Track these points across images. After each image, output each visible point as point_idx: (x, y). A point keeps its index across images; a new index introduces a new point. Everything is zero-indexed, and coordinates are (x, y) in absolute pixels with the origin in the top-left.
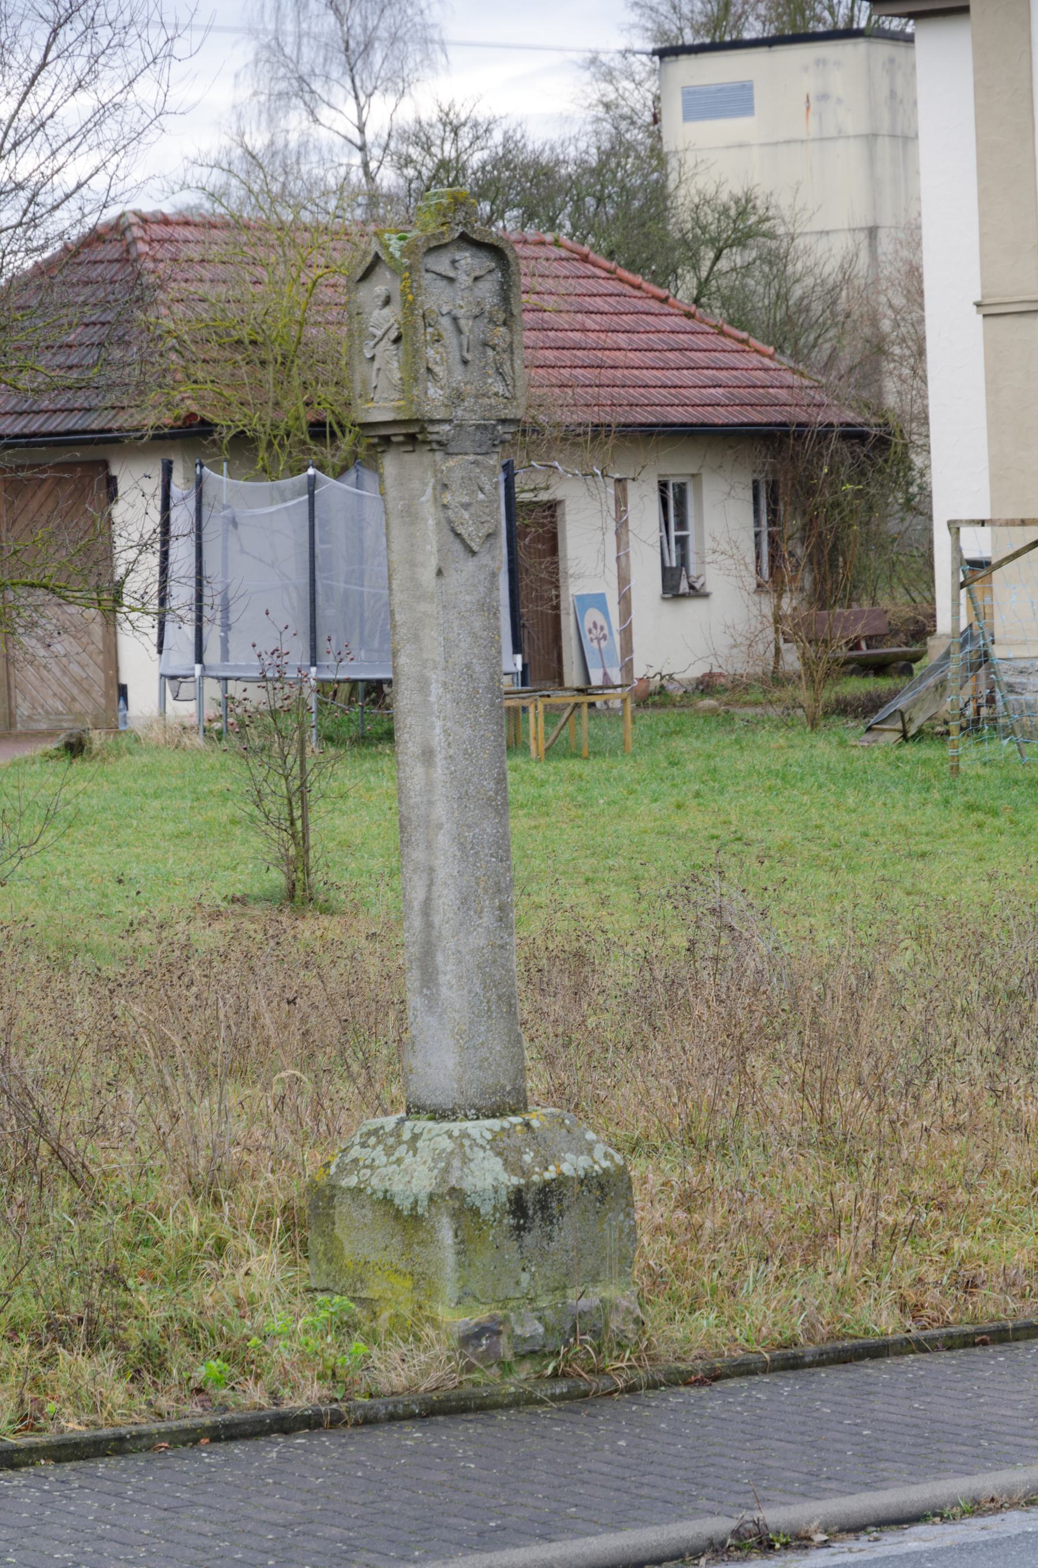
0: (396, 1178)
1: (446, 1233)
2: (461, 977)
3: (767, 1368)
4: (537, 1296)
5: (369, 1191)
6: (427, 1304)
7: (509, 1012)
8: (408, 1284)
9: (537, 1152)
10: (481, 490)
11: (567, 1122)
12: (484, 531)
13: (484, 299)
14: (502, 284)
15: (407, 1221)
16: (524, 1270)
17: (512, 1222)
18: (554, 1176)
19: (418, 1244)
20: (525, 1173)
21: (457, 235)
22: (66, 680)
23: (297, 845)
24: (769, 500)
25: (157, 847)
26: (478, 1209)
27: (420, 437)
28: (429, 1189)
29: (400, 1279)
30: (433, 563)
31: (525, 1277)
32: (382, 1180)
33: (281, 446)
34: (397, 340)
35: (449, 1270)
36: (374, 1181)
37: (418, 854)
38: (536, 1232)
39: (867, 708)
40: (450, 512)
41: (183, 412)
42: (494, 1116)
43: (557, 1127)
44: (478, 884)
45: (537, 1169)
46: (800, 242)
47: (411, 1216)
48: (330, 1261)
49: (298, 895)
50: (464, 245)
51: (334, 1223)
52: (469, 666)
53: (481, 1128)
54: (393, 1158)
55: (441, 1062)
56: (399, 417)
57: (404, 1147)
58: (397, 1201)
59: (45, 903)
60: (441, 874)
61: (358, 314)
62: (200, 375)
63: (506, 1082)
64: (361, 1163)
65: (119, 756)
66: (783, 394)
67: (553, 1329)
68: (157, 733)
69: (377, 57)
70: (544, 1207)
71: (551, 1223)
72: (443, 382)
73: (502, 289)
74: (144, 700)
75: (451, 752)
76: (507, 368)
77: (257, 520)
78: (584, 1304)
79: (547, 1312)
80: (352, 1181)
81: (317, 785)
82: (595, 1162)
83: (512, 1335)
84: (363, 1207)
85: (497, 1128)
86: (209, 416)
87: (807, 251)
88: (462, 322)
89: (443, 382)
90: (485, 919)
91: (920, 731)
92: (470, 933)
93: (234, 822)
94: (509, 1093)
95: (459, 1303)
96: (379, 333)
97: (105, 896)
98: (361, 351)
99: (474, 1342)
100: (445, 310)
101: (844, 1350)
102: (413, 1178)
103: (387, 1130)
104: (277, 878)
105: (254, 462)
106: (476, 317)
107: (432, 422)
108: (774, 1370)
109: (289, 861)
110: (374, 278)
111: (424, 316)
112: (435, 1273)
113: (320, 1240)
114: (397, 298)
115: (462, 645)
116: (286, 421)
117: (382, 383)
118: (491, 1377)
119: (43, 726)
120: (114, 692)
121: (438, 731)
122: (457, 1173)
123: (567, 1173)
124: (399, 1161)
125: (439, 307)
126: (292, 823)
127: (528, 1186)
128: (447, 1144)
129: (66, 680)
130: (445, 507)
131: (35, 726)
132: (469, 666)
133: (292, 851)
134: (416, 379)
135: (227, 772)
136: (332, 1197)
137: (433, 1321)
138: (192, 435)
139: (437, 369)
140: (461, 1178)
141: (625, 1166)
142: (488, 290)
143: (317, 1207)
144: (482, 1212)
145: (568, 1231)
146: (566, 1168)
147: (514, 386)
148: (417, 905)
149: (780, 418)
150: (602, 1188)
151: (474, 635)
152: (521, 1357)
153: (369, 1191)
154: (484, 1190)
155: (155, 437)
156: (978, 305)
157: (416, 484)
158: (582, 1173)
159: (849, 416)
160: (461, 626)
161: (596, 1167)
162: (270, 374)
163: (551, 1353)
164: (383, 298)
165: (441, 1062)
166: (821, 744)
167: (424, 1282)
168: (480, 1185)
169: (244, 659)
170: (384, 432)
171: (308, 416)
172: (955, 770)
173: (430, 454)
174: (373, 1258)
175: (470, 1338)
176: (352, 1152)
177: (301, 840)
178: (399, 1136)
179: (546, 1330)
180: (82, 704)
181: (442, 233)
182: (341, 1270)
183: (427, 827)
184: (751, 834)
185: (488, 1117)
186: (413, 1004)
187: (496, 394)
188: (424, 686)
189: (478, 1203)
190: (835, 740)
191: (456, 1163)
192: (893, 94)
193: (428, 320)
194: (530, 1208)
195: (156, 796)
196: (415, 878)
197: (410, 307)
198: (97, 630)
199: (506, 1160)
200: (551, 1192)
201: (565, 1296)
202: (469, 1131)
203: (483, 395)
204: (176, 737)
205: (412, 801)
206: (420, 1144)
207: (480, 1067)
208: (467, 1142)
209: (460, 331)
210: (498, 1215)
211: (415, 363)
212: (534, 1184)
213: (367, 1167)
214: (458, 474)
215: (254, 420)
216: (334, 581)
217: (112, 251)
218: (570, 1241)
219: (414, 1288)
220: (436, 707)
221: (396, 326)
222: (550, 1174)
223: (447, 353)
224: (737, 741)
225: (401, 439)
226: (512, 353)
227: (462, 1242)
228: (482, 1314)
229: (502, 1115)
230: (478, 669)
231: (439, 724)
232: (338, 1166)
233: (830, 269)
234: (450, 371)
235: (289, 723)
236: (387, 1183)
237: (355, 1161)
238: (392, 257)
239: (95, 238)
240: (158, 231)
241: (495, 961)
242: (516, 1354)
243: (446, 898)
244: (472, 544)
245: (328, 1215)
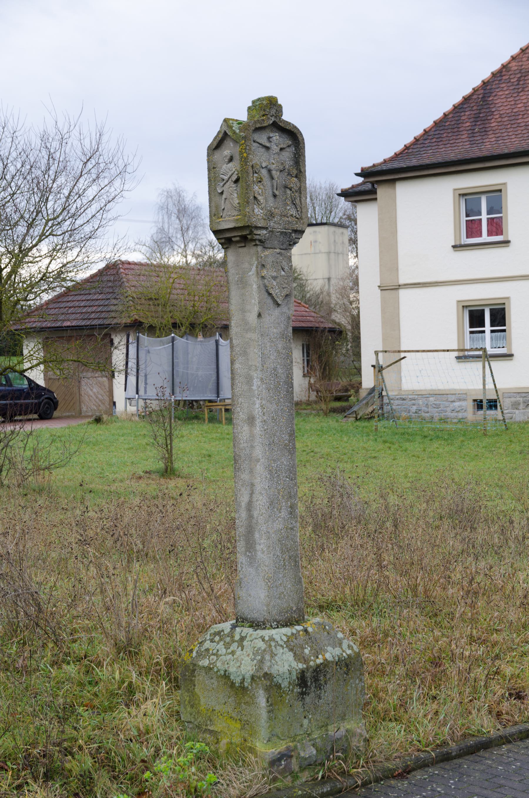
0: (232, 663)
1: (262, 700)
2: (269, 547)
3: (434, 762)
4: (312, 731)
5: (215, 670)
6: (249, 739)
7: (295, 566)
8: (238, 726)
9: (311, 647)
10: (283, 269)
11: (327, 627)
12: (284, 293)
13: (285, 161)
14: (295, 154)
15: (239, 690)
16: (305, 717)
17: (299, 690)
18: (322, 661)
19: (245, 703)
20: (306, 661)
21: (271, 122)
22: (97, 400)
23: (168, 453)
24: (307, 350)
25: (122, 453)
26: (280, 685)
27: (249, 237)
28: (251, 673)
29: (233, 722)
30: (256, 310)
31: (306, 722)
32: (223, 664)
33: (163, 329)
34: (237, 181)
35: (263, 721)
36: (219, 664)
37: (245, 476)
38: (312, 695)
39: (342, 410)
40: (266, 281)
41: (134, 319)
42: (287, 626)
43: (322, 631)
44: (279, 493)
45: (312, 658)
46: (309, 282)
47: (240, 687)
48: (192, 706)
49: (168, 472)
50: (275, 129)
51: (195, 686)
52: (275, 369)
53: (280, 634)
54: (229, 651)
55: (257, 594)
56: (237, 226)
57: (235, 645)
58: (232, 677)
59: (82, 472)
60: (258, 488)
61: (214, 168)
62: (139, 308)
63: (293, 605)
64: (211, 652)
65: (112, 423)
66: (311, 319)
67: (321, 750)
68: (124, 416)
69: (190, 232)
70: (316, 679)
71: (320, 688)
72: (263, 206)
73: (295, 157)
74: (120, 406)
75: (265, 418)
76: (298, 201)
77: (156, 352)
78: (338, 735)
79: (317, 741)
80: (205, 662)
81: (175, 433)
82: (343, 651)
83: (298, 757)
84: (212, 678)
85: (289, 634)
86: (141, 320)
87: (311, 284)
88: (274, 172)
89: (263, 206)
90: (283, 513)
91: (360, 418)
92: (274, 521)
93: (147, 444)
94: (295, 611)
95: (269, 741)
96: (226, 178)
97: (103, 470)
98: (215, 189)
99: (277, 763)
100: (264, 165)
101: (471, 746)
102: (242, 664)
103: (226, 633)
104: (161, 465)
105: (155, 334)
106: (281, 171)
107: (257, 228)
108: (437, 763)
109: (166, 459)
110: (223, 147)
111: (252, 166)
112: (255, 722)
113: (186, 694)
114: (237, 157)
115: (272, 357)
116: (165, 322)
117: (228, 206)
118: (287, 783)
119: (90, 414)
120: (112, 404)
121: (257, 406)
122: (268, 664)
123: (329, 659)
124: (233, 653)
125: (261, 163)
126: (167, 446)
127: (307, 668)
128: (261, 645)
129: (97, 400)
130: (263, 277)
131: (87, 414)
132: (275, 369)
133: (167, 456)
134: (248, 202)
135: (145, 428)
136: (194, 670)
137: (252, 750)
138: (136, 326)
139: (259, 198)
140: (271, 666)
141: (359, 653)
142: (287, 156)
143: (185, 675)
144: (282, 686)
145: (328, 694)
146: (328, 656)
147: (301, 212)
148: (243, 504)
149: (311, 326)
150: (347, 666)
151: (278, 352)
152: (302, 769)
153: (215, 670)
154: (284, 673)
155: (125, 326)
156: (379, 287)
157: (246, 265)
158: (337, 658)
159: (330, 325)
160: (271, 346)
161: (344, 654)
162: (160, 308)
163: (320, 764)
164: (228, 157)
165: (257, 594)
166: (331, 421)
167: (247, 725)
168: (281, 670)
169: (152, 393)
170: (228, 235)
171: (171, 321)
172: (376, 429)
173: (255, 248)
174: (217, 708)
175: (274, 762)
176: (205, 644)
177: (170, 452)
178: (233, 637)
179: (317, 751)
180: (102, 407)
181: (263, 120)
182: (198, 712)
183: (251, 461)
184: (316, 450)
185: (283, 626)
186: (241, 560)
187: (292, 215)
188: (249, 380)
189: (280, 681)
190: (335, 420)
191: (267, 657)
192: (335, 241)
193: (255, 169)
194: (308, 681)
195: (123, 436)
196: (243, 489)
197: (244, 161)
198: (106, 383)
199: (295, 653)
200: (320, 671)
201: (327, 730)
202: (274, 636)
203: (284, 216)
204: (130, 418)
205: (241, 446)
206: (245, 643)
207: (279, 598)
208: (273, 644)
209: (272, 178)
210: (291, 687)
211: (247, 193)
212: (311, 667)
213: (214, 654)
214: (270, 260)
215: (155, 322)
216: (180, 369)
217: (112, 272)
218: (330, 698)
219: (242, 729)
220: (256, 392)
221: (236, 173)
222: (319, 661)
223: (265, 190)
224: (304, 420)
225: (238, 239)
226: (300, 193)
227: (271, 705)
228: (282, 747)
229: (291, 624)
230: (280, 371)
231: (258, 402)
232: (197, 652)
233: (318, 289)
234: (266, 199)
235: (165, 413)
236: (226, 666)
237: (207, 650)
238: (234, 133)
239: (108, 268)
240: (126, 266)
241: (288, 537)
242: (300, 767)
243: (261, 502)
244: (278, 300)
245: (191, 680)
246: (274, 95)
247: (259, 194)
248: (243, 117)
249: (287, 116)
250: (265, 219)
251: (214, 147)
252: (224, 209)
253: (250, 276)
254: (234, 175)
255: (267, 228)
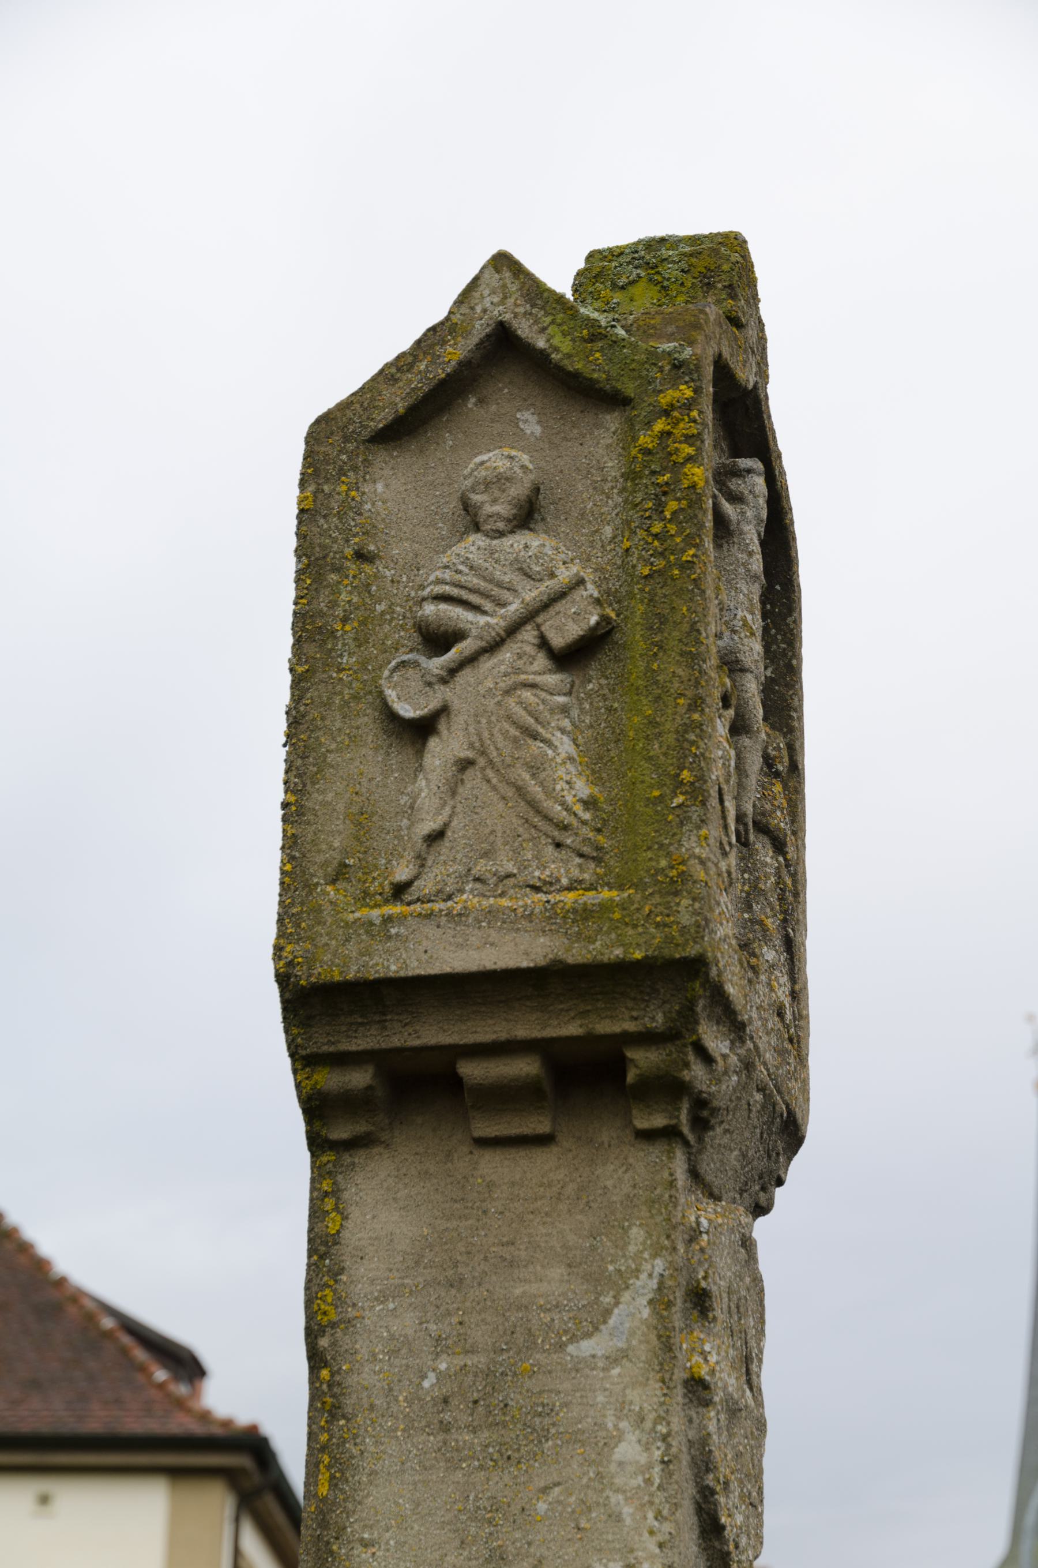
56: (578, 954)
157: (550, 1283)
170: (432, 1032)
246: (494, 251)
248: (559, 276)
251: (381, 419)
252: (436, 837)
253: (578, 1366)
254: (567, 607)
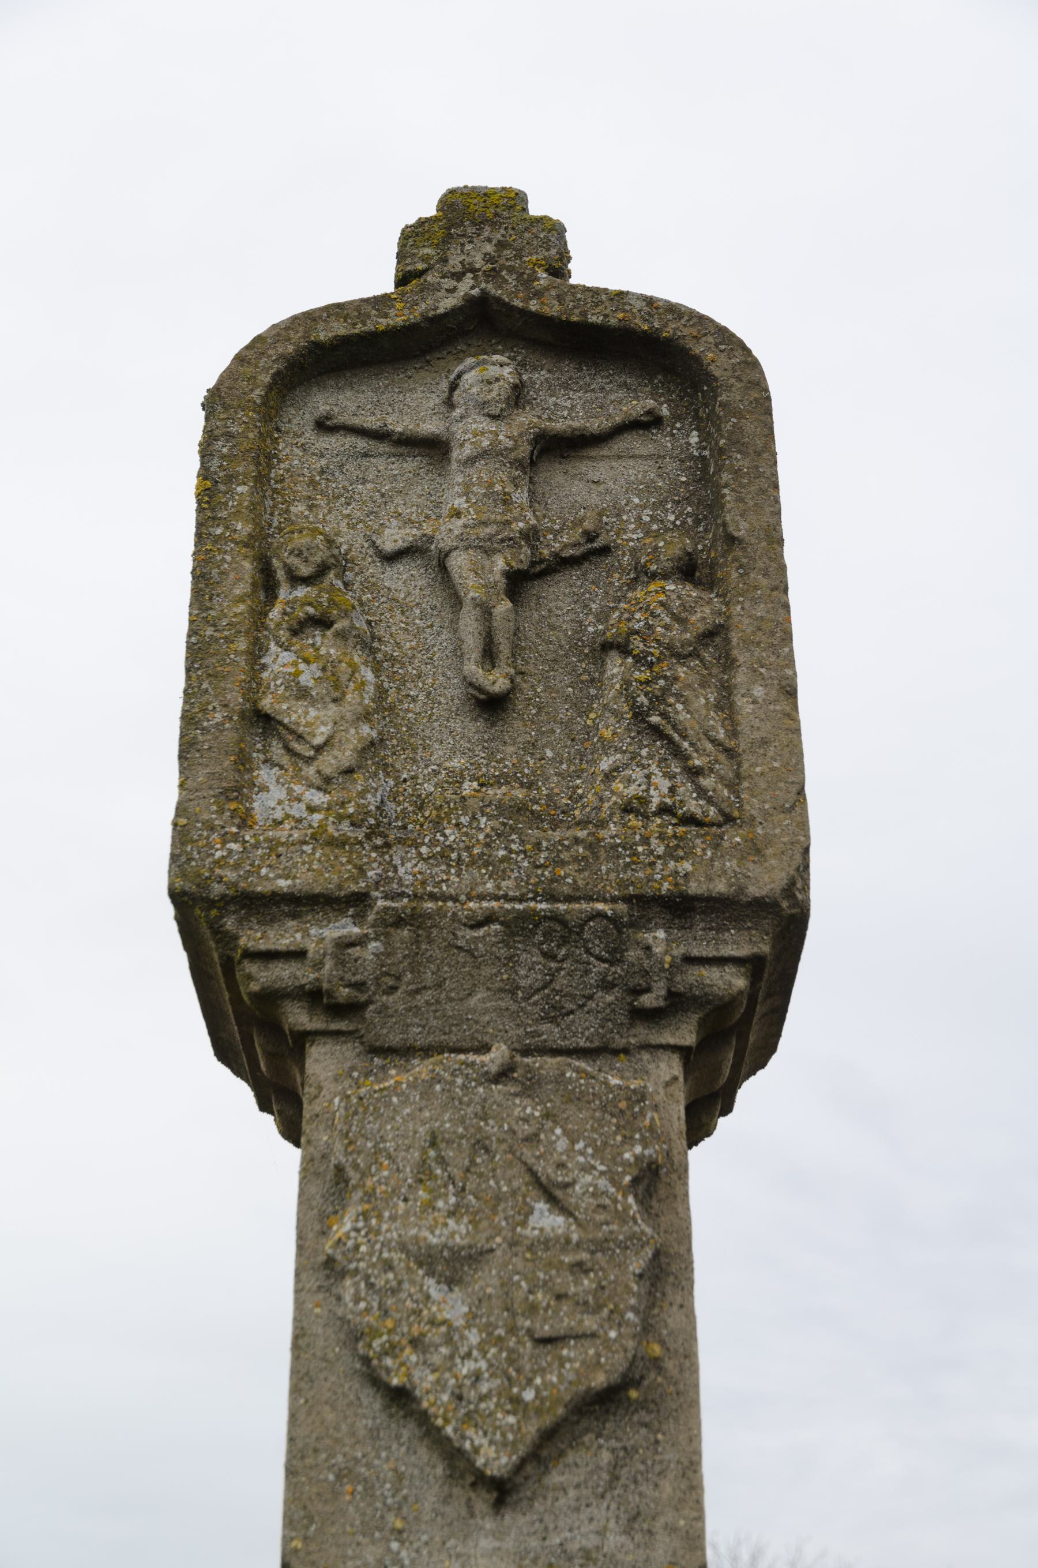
247: (303, 693)
249: (603, 262)
250: (334, 843)
255: (359, 901)
